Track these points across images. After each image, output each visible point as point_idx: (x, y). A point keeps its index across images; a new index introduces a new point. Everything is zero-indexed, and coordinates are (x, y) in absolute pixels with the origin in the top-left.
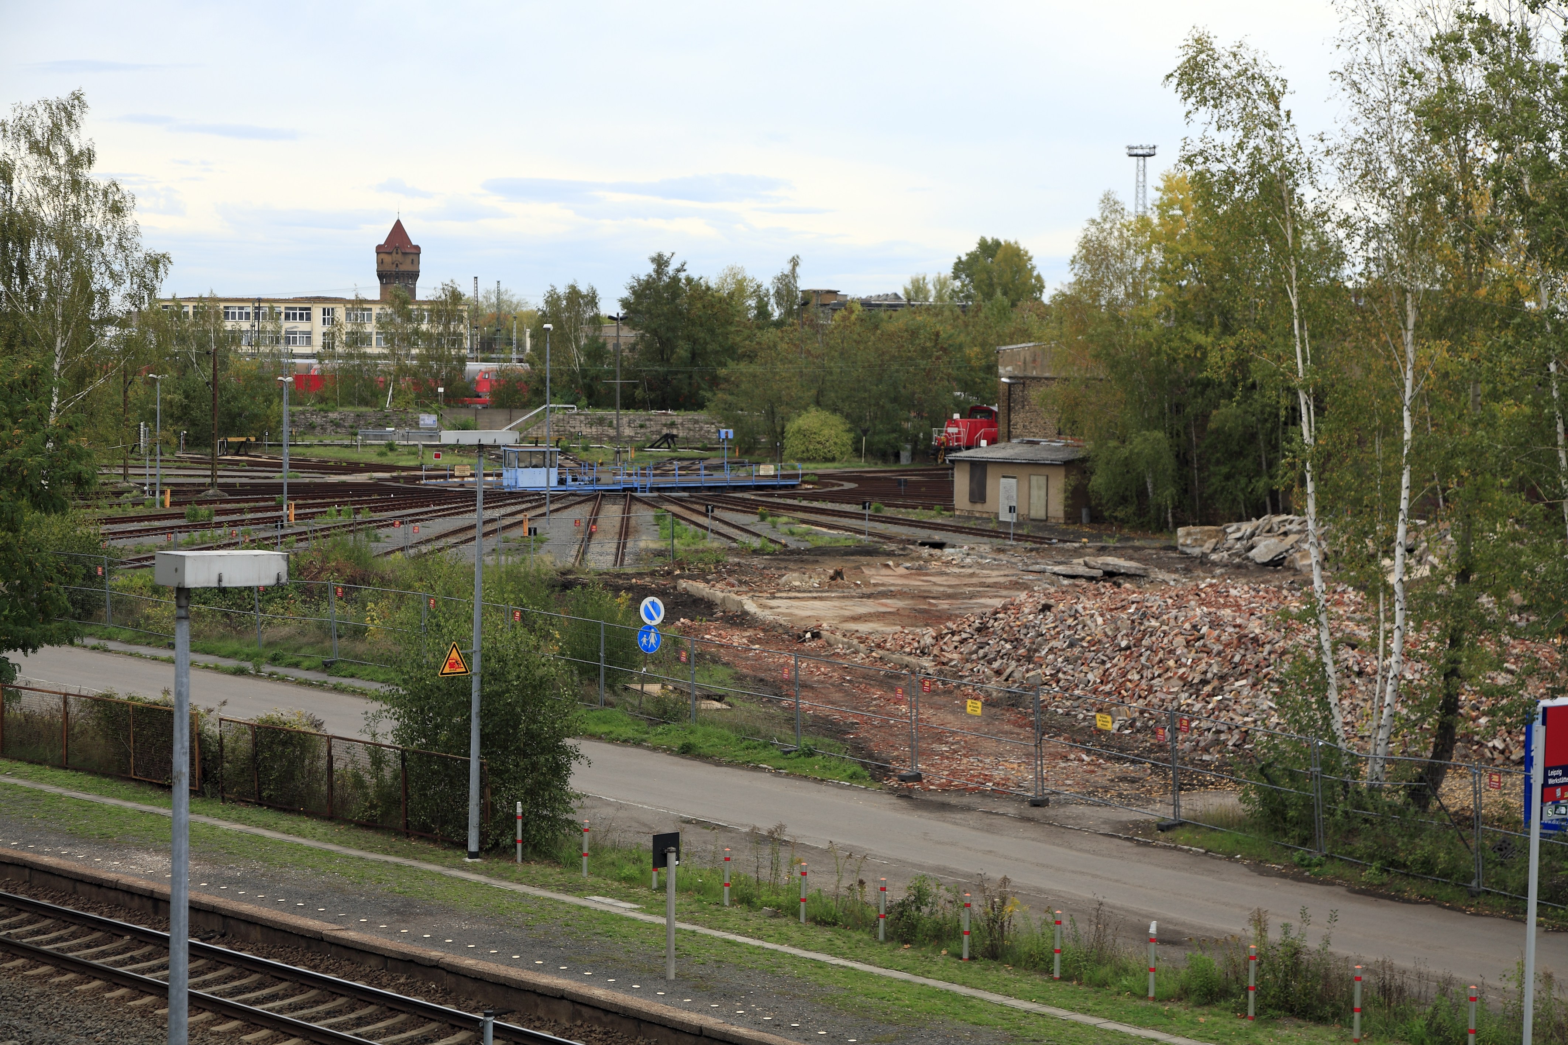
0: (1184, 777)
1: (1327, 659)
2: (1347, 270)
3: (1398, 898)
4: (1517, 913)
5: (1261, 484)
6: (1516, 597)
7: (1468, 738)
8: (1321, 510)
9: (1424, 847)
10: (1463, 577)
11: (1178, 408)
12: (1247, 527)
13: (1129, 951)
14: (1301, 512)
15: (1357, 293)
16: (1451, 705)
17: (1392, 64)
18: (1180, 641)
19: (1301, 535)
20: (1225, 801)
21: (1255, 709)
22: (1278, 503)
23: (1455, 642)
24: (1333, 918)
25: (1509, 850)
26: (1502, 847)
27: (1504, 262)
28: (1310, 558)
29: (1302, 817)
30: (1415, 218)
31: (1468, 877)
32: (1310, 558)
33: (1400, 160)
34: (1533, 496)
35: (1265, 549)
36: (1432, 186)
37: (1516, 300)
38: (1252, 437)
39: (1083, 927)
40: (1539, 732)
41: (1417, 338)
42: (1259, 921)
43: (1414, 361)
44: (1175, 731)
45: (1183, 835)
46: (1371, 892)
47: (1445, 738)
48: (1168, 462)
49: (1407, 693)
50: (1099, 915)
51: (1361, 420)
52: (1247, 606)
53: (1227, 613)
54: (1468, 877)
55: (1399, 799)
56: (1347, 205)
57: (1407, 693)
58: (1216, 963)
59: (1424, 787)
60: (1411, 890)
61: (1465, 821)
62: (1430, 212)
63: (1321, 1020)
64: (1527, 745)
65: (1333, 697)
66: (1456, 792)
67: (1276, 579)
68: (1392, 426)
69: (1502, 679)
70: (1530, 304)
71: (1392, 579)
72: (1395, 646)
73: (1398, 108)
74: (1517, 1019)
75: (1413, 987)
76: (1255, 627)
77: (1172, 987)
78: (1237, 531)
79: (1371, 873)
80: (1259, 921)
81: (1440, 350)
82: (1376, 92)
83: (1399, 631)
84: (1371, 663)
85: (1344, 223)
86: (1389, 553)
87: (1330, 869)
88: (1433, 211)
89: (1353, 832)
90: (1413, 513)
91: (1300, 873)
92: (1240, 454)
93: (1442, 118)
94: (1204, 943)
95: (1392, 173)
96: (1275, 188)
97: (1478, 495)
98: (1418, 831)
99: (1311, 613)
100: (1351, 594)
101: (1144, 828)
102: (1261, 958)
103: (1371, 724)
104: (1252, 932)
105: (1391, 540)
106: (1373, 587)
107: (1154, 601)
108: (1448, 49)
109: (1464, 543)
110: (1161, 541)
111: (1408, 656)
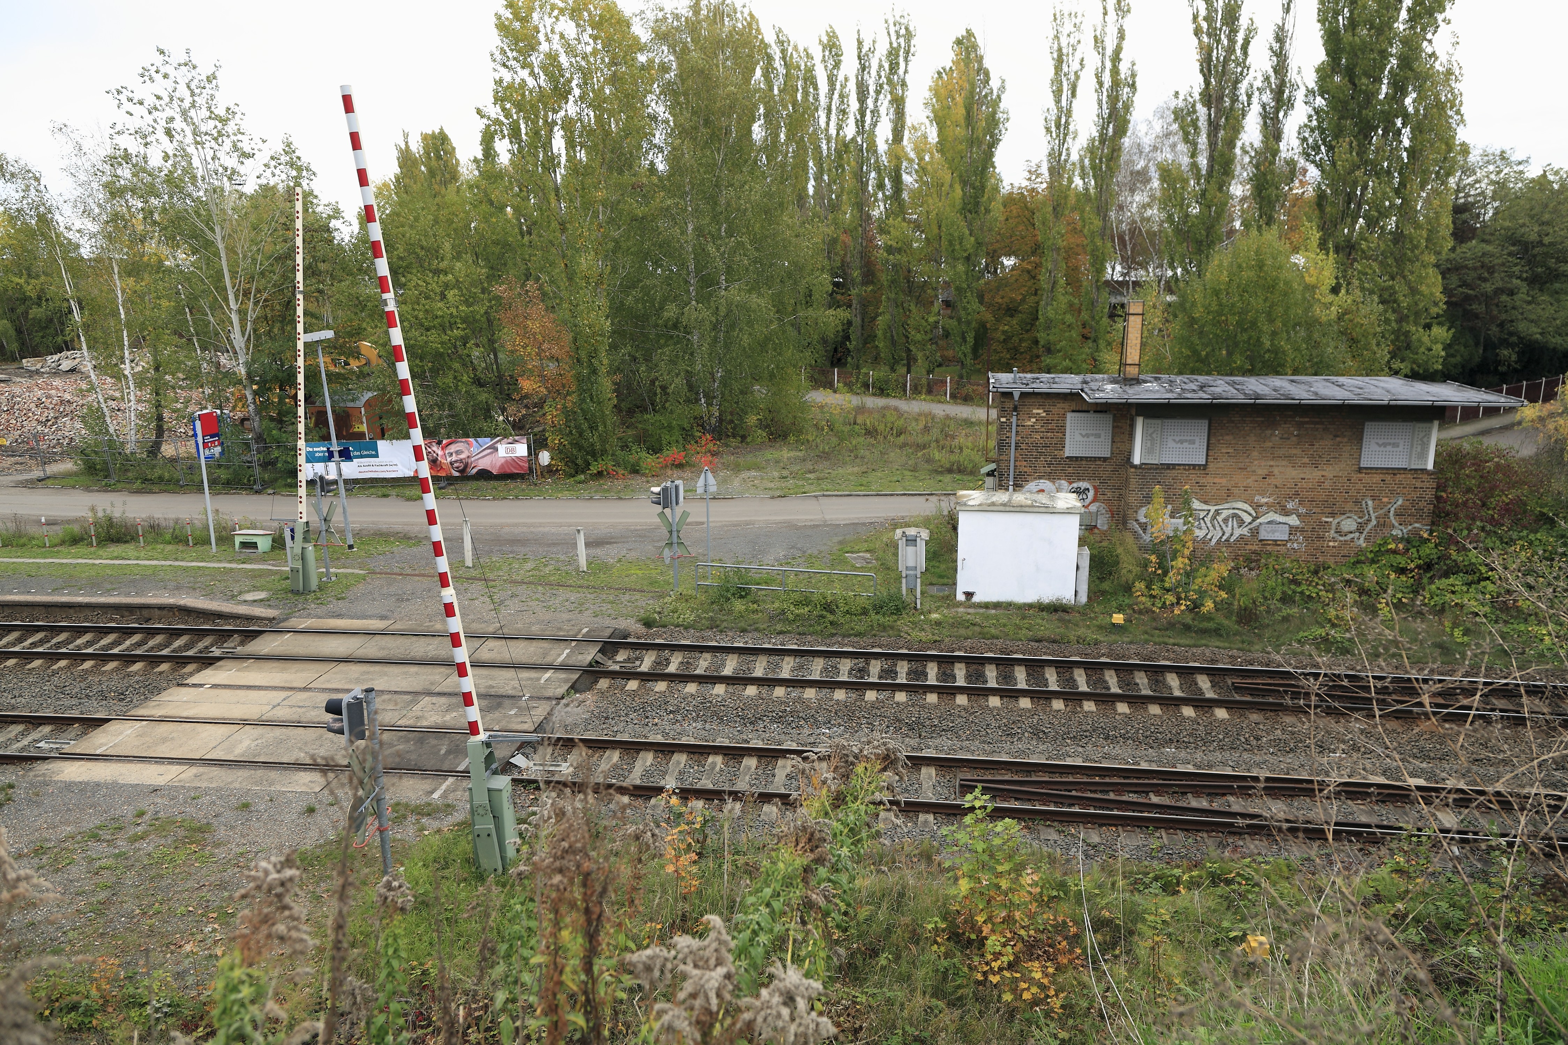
0: (47, 459)
1: (103, 405)
2: (82, 250)
3: (151, 492)
4: (201, 490)
5: (59, 339)
6: (181, 375)
7: (169, 430)
8: (89, 348)
9: (158, 472)
10: (157, 369)
11: (13, 310)
12: (56, 357)
13: (33, 530)
14: (80, 349)
15: (90, 260)
16: (160, 418)
17: (88, 165)
18: (33, 406)
19: (83, 358)
20: (68, 466)
21: (74, 429)
22: (68, 346)
23: (157, 394)
24: (125, 503)
25: (193, 468)
26: (190, 468)
27: (151, 246)
28: (88, 367)
29: (102, 467)
30: (110, 229)
31: (178, 481)
32: (88, 367)
33: (100, 206)
34: (181, 336)
35: (66, 365)
36: (115, 217)
37: (160, 262)
38: (51, 320)
39: (9, 524)
40: (198, 424)
41: (120, 277)
42: (93, 509)
43: (120, 287)
44: (37, 442)
45: (49, 482)
46: (138, 492)
47: (160, 431)
48: (12, 332)
49: (141, 415)
50: (16, 518)
51: (98, 309)
52: (62, 389)
53: (53, 392)
54: (178, 481)
55: (144, 456)
56: (78, 225)
57: (141, 415)
58: (76, 529)
59: (154, 449)
60: (155, 488)
61: (173, 460)
62: (116, 227)
63: (126, 542)
64: (194, 429)
65: (108, 420)
66: (167, 450)
67: (73, 377)
68: (115, 314)
69: (179, 406)
70: (167, 263)
71: (126, 372)
72: (132, 398)
73: (95, 185)
74: (207, 528)
75: (163, 524)
76: (67, 397)
77: (57, 541)
78: (51, 359)
79: (138, 484)
80: (93, 509)
81: (131, 281)
82: (83, 177)
83: (133, 393)
84: (123, 406)
85: (79, 231)
86: (123, 363)
87: (119, 486)
88: (116, 225)
89: (127, 470)
90: (130, 346)
91: (107, 489)
92: (46, 327)
93: (114, 191)
94: (68, 522)
95: (97, 211)
96: (45, 220)
97: (158, 338)
98: (154, 467)
99: (92, 388)
100: (109, 380)
101: (31, 481)
102: (95, 524)
103: (128, 425)
104: (90, 514)
105: (123, 358)
106: (119, 376)
107: (17, 390)
108: (112, 160)
109: (155, 355)
110: (16, 365)
111: (139, 401)
